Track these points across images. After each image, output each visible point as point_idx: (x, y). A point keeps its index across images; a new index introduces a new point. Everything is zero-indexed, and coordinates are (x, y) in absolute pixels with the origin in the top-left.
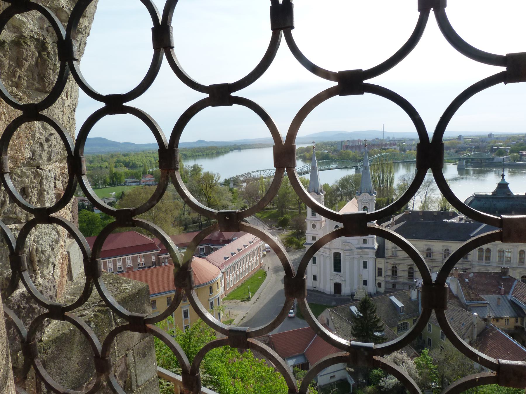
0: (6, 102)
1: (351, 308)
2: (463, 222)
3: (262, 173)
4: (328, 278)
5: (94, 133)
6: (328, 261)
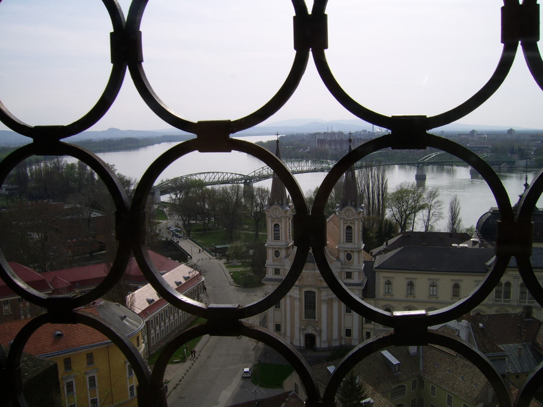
0: (478, 303)
1: (328, 368)
2: (477, 246)
3: (208, 176)
4: (297, 326)
5: (29, 348)
6: (297, 303)
